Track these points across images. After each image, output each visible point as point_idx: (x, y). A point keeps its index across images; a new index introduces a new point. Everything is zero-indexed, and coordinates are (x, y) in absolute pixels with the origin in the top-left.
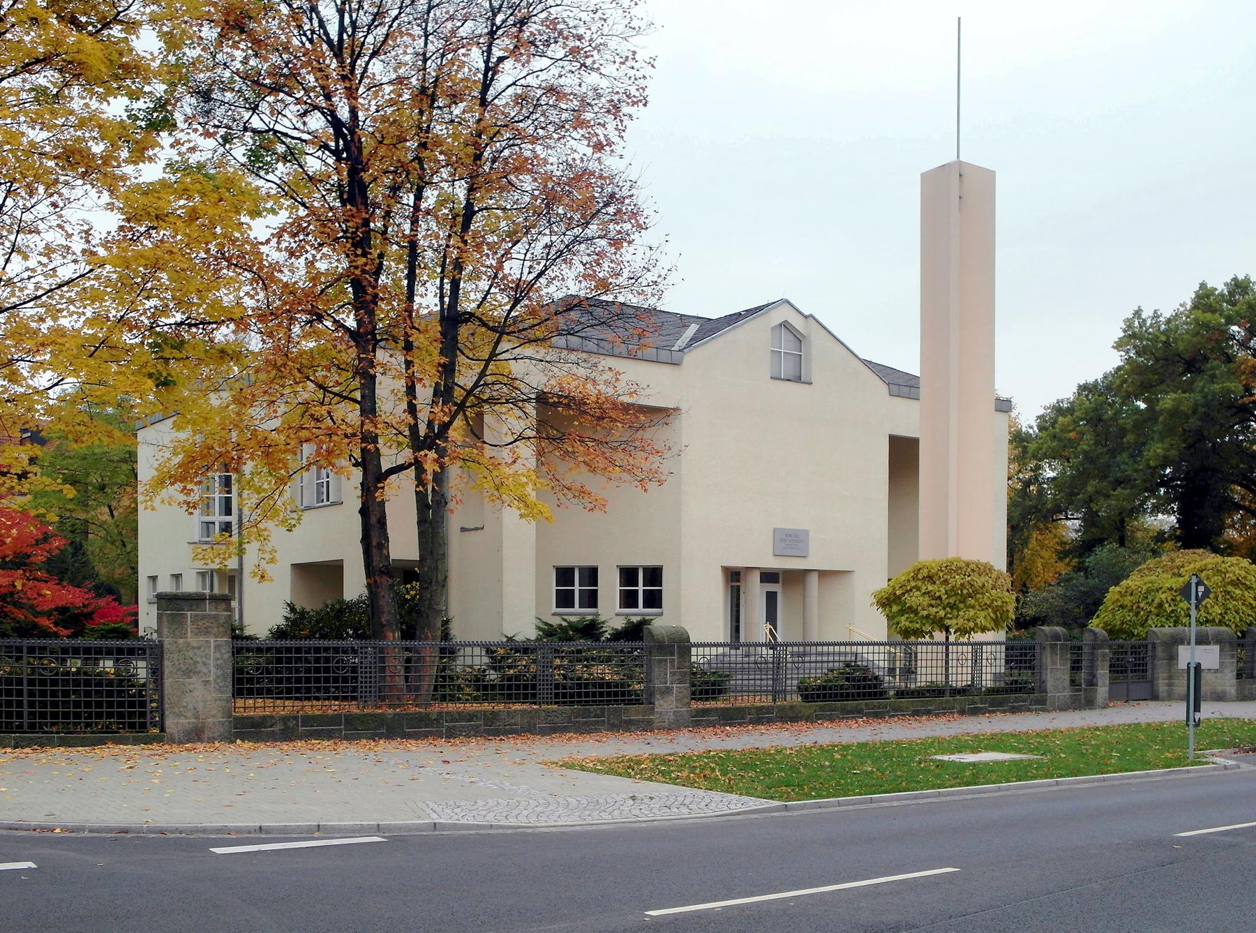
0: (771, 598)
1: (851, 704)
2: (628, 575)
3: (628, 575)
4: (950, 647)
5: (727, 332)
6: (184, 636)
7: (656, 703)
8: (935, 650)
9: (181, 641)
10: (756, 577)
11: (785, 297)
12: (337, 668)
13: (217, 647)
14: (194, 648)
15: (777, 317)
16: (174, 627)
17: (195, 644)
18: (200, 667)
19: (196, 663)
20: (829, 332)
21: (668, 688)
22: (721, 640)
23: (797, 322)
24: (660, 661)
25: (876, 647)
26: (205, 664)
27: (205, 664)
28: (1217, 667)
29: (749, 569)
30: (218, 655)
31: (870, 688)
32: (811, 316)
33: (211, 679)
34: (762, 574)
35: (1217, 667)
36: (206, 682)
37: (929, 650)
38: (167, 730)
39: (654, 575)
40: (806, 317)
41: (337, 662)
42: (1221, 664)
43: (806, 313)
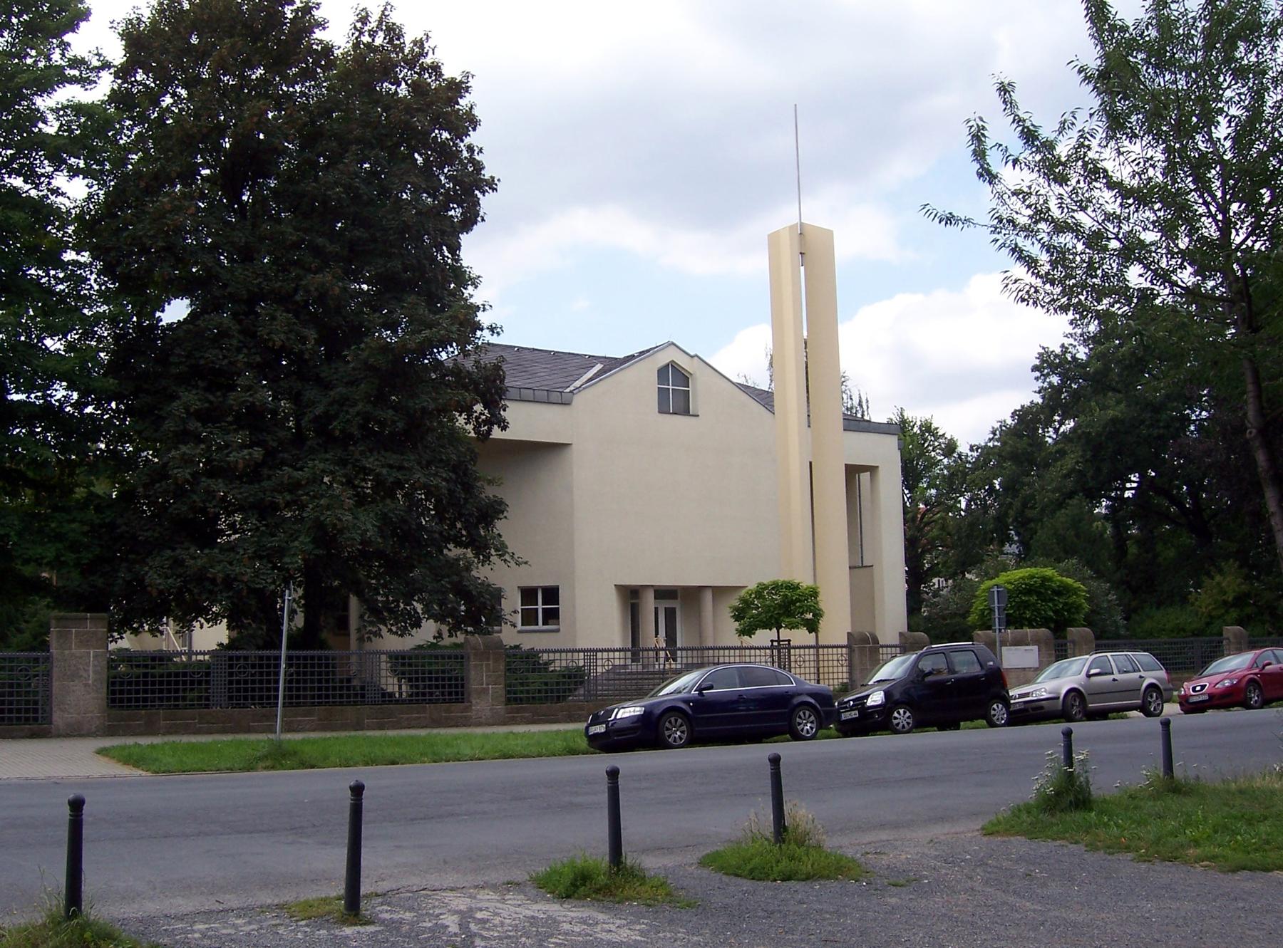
0: (670, 614)
1: (544, 707)
2: (528, 594)
3: (528, 594)
4: (792, 651)
5: (615, 373)
6: (70, 649)
7: (474, 702)
8: (835, 652)
9: (67, 652)
10: (650, 596)
11: (671, 340)
12: (240, 672)
13: (95, 657)
14: (76, 657)
15: (663, 359)
16: (61, 641)
17: (78, 655)
18: (82, 673)
19: (79, 669)
20: (716, 371)
21: (484, 688)
22: (618, 645)
23: (683, 362)
24: (476, 666)
25: (830, 650)
26: (85, 670)
27: (85, 670)
28: (1037, 665)
29: (701, 589)
30: (96, 663)
31: (515, 694)
32: (696, 356)
33: (90, 682)
34: (656, 591)
35: (1037, 665)
36: (86, 685)
37: (835, 652)
38: (55, 723)
39: (552, 594)
40: (692, 357)
41: (239, 668)
42: (1040, 662)
43: (692, 354)
